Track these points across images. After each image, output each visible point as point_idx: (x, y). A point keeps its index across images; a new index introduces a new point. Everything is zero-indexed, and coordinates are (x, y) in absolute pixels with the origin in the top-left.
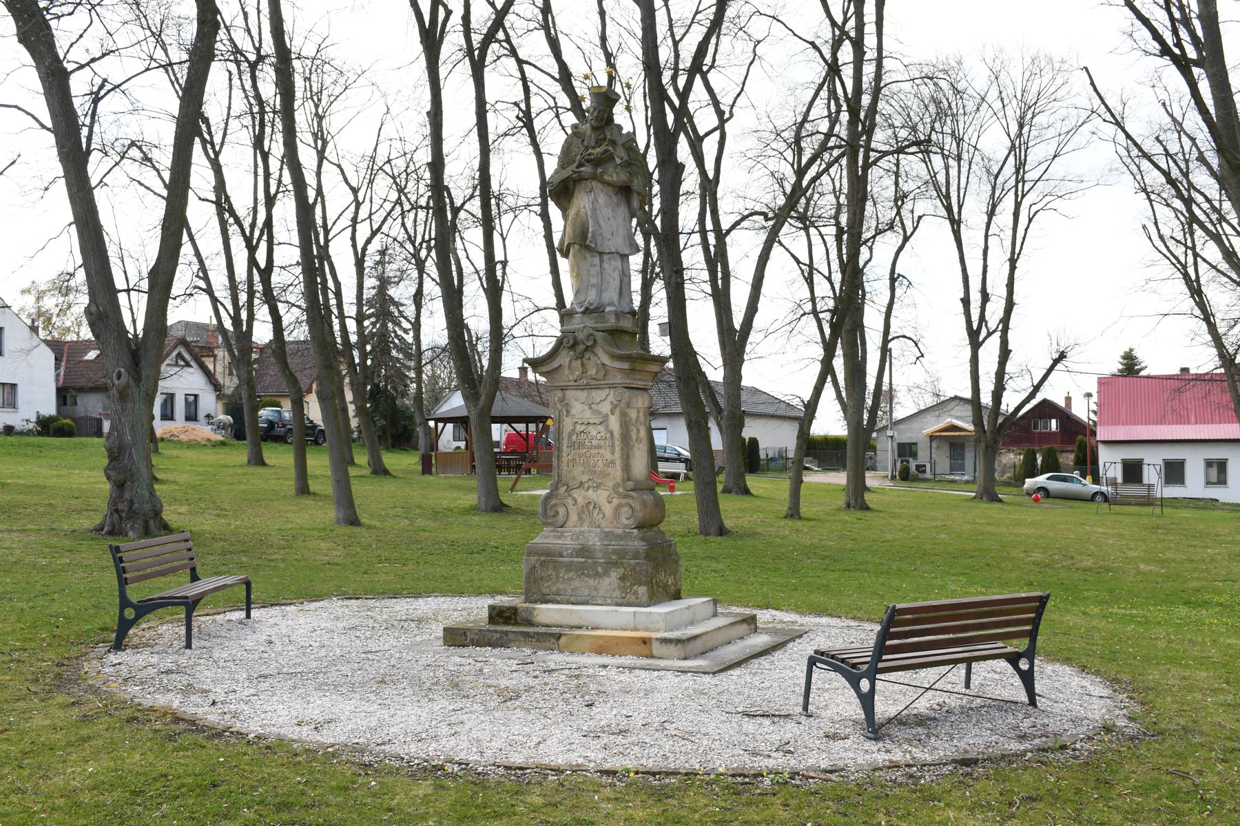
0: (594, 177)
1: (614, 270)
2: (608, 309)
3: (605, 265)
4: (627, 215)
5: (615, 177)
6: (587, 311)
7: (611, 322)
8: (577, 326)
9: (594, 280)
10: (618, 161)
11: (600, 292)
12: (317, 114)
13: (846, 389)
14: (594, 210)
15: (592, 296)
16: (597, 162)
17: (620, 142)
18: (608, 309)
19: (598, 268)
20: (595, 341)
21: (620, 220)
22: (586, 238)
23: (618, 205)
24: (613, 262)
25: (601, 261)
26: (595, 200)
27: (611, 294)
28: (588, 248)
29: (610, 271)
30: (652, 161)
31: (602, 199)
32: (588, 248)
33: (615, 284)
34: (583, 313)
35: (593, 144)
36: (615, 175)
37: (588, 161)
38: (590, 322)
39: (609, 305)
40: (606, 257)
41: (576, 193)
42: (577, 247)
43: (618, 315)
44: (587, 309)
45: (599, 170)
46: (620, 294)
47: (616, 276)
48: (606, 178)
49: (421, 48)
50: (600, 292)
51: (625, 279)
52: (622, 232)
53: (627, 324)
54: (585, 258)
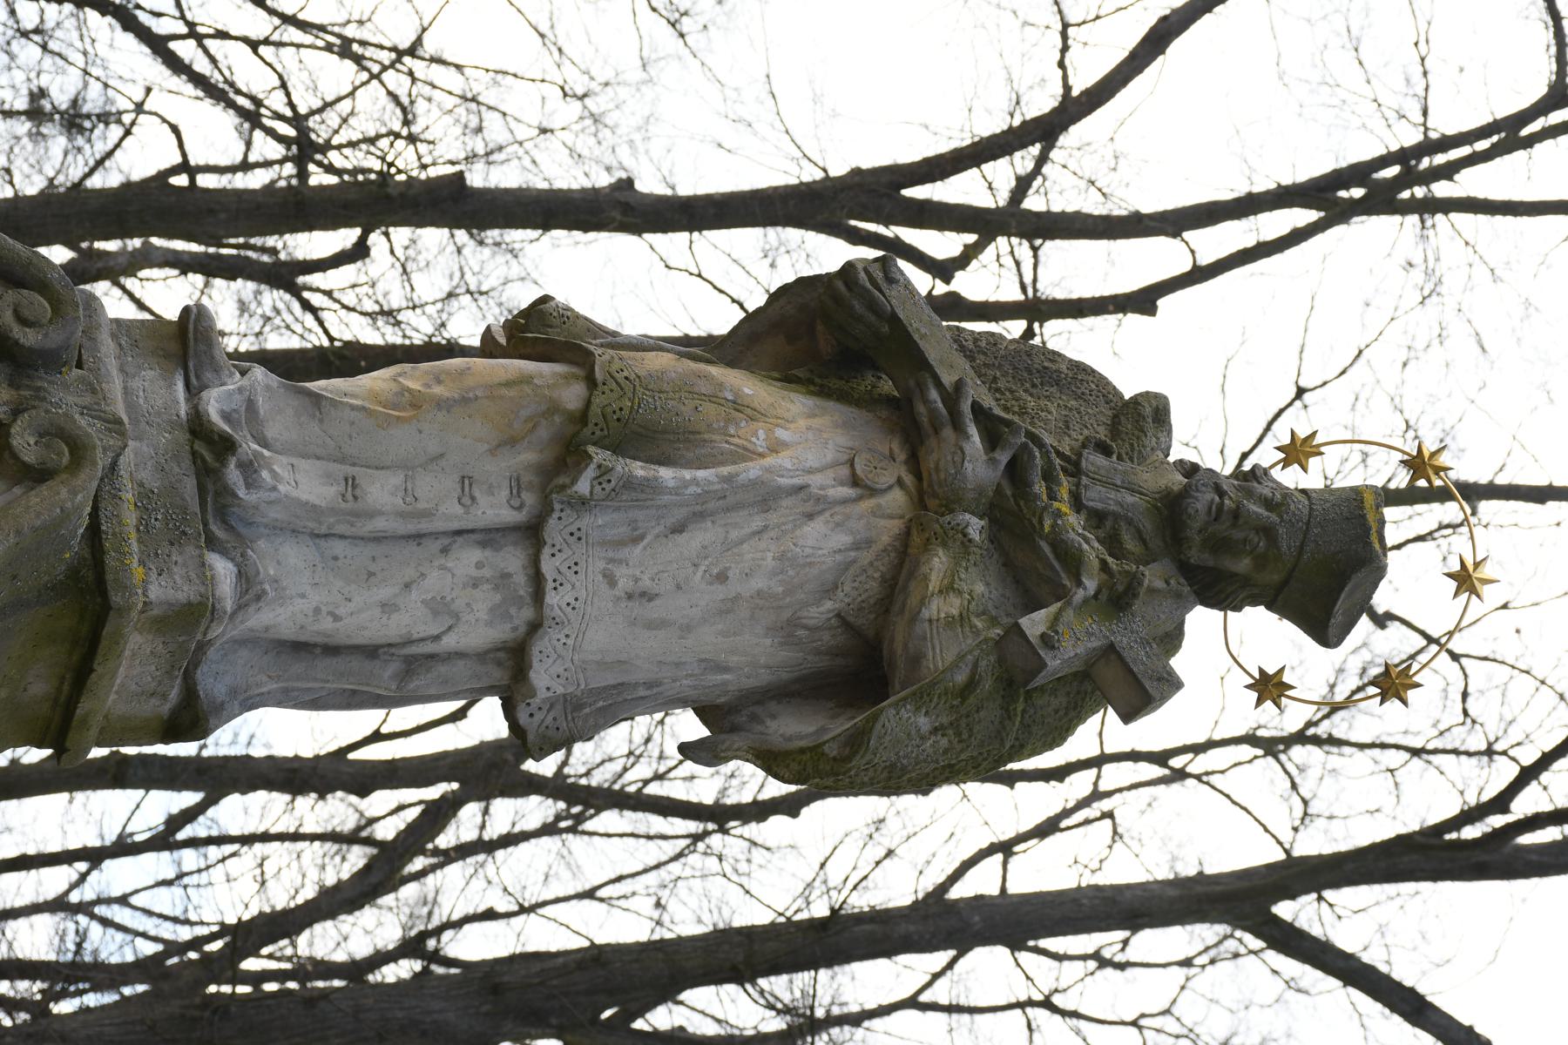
0: (931, 501)
1: (438, 607)
2: (223, 568)
3: (468, 559)
4: (731, 682)
5: (941, 607)
6: (209, 447)
7: (153, 584)
8: (115, 386)
9: (381, 491)
10: (1034, 624)
11: (313, 528)
12: (371, 315)
13: (208, 245)
14: (766, 497)
15: (293, 479)
16: (1013, 519)
17: (1127, 636)
18: (223, 568)
19: (451, 514)
20: (38, 475)
21: (709, 640)
22: (618, 449)
23: (788, 630)
24: (483, 601)
25: (489, 537)
26: (815, 507)
27: (302, 593)
28: (568, 455)
29: (435, 582)
30: (186, 749)
31: (823, 541)
32: (568, 455)
33: (362, 612)
34: (198, 427)
35: (1095, 496)
36: (955, 600)
37: (1016, 471)
38: (144, 460)
39: (245, 578)
40: (513, 560)
41: (836, 411)
42: (573, 396)
43: (189, 621)
44: (225, 446)
45: (975, 526)
46: (299, 648)
47: (409, 620)
48: (938, 564)
49: (838, 170)
50: (313, 528)
51: (387, 672)
52: (647, 651)
53: (132, 670)
54: (511, 442)
